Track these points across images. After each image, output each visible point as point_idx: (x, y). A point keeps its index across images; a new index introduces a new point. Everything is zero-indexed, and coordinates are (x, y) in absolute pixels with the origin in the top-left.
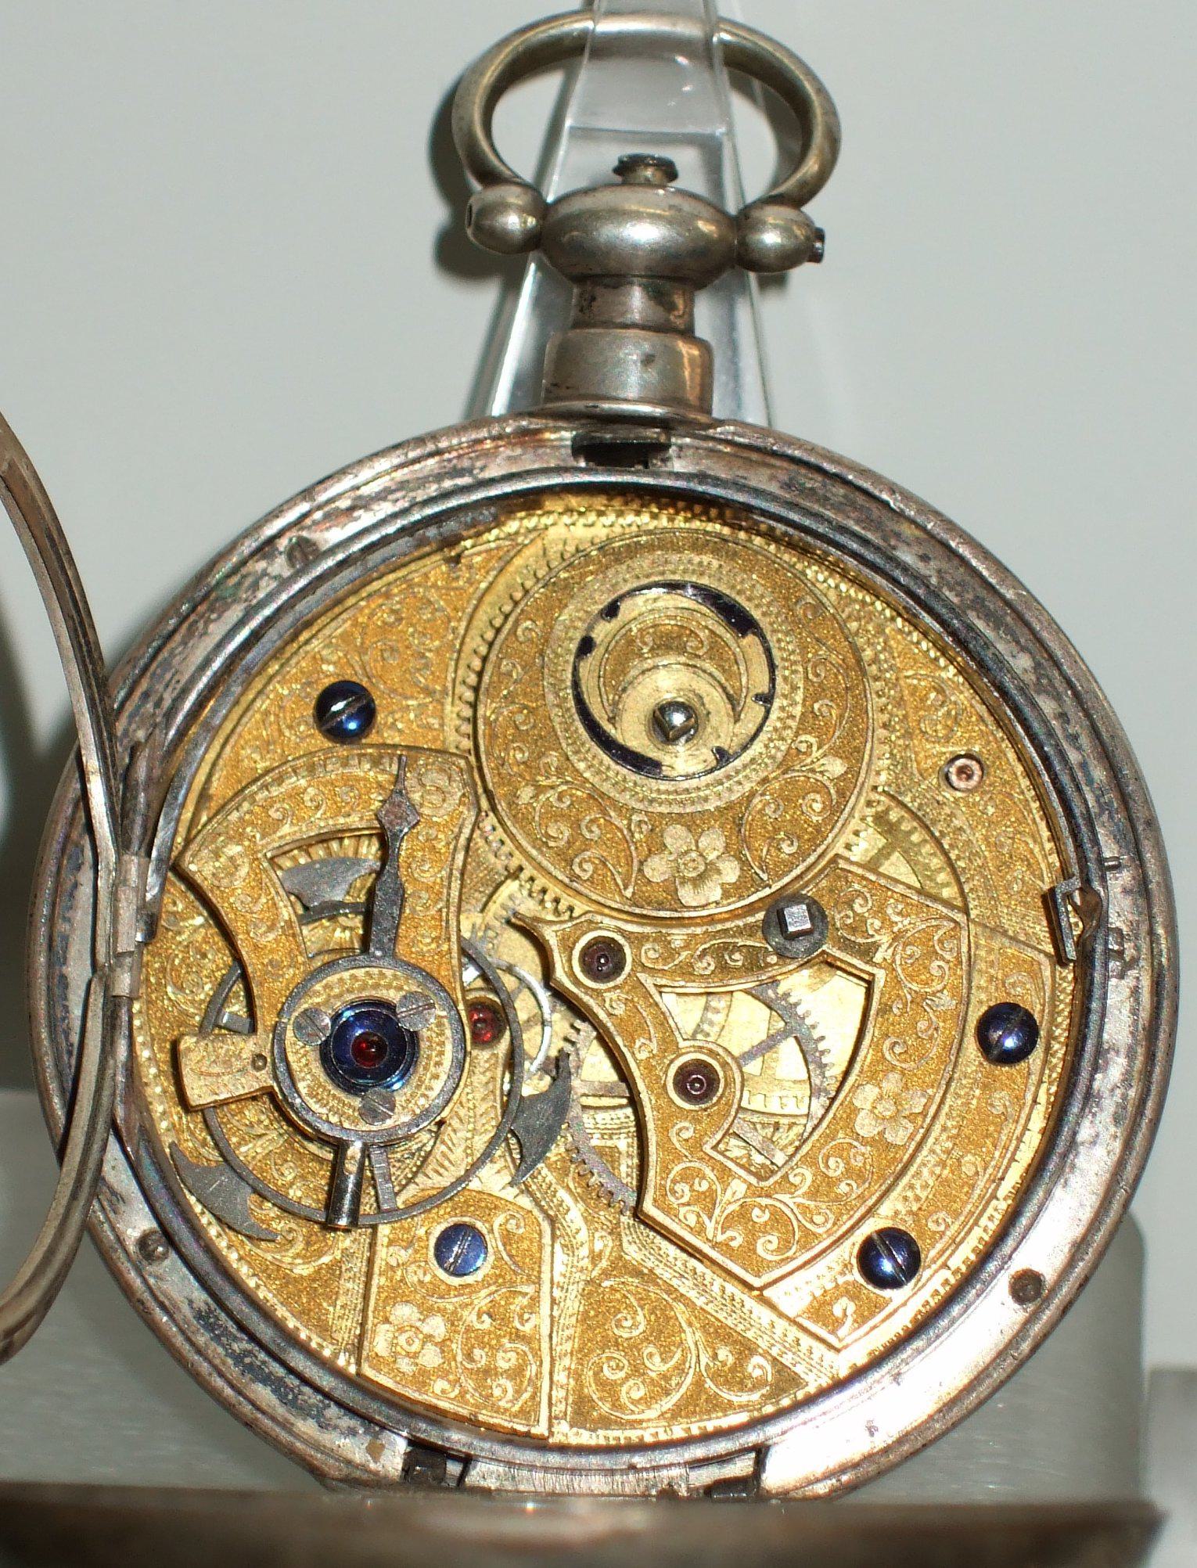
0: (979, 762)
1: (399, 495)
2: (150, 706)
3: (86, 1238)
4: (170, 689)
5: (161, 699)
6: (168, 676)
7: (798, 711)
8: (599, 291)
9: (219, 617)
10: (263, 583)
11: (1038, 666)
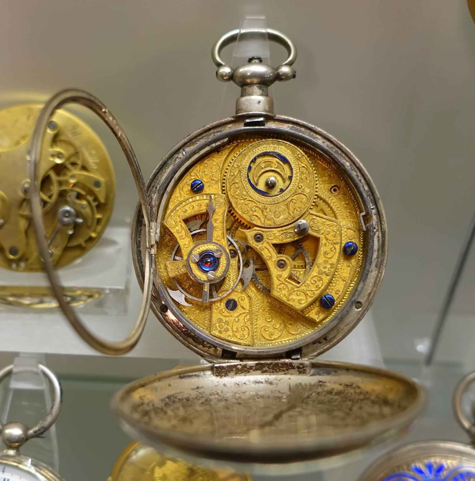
0: (337, 187)
1: (206, 137)
2: (154, 189)
3: (147, 178)
4: (158, 185)
5: (157, 187)
6: (158, 182)
7: (298, 178)
8: (247, 87)
9: (168, 168)
10: (177, 160)
11: (351, 165)
